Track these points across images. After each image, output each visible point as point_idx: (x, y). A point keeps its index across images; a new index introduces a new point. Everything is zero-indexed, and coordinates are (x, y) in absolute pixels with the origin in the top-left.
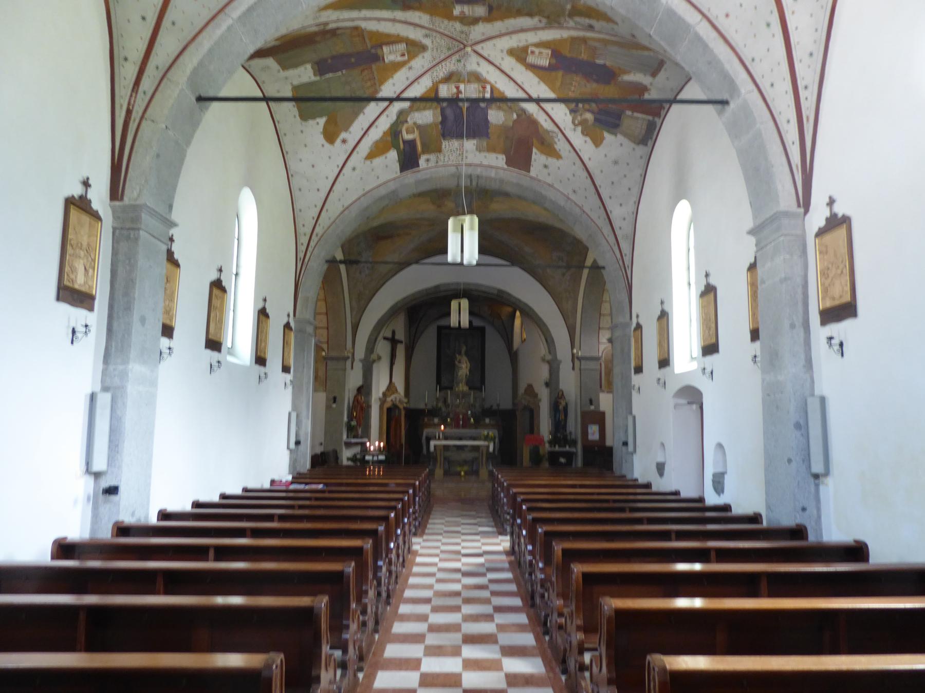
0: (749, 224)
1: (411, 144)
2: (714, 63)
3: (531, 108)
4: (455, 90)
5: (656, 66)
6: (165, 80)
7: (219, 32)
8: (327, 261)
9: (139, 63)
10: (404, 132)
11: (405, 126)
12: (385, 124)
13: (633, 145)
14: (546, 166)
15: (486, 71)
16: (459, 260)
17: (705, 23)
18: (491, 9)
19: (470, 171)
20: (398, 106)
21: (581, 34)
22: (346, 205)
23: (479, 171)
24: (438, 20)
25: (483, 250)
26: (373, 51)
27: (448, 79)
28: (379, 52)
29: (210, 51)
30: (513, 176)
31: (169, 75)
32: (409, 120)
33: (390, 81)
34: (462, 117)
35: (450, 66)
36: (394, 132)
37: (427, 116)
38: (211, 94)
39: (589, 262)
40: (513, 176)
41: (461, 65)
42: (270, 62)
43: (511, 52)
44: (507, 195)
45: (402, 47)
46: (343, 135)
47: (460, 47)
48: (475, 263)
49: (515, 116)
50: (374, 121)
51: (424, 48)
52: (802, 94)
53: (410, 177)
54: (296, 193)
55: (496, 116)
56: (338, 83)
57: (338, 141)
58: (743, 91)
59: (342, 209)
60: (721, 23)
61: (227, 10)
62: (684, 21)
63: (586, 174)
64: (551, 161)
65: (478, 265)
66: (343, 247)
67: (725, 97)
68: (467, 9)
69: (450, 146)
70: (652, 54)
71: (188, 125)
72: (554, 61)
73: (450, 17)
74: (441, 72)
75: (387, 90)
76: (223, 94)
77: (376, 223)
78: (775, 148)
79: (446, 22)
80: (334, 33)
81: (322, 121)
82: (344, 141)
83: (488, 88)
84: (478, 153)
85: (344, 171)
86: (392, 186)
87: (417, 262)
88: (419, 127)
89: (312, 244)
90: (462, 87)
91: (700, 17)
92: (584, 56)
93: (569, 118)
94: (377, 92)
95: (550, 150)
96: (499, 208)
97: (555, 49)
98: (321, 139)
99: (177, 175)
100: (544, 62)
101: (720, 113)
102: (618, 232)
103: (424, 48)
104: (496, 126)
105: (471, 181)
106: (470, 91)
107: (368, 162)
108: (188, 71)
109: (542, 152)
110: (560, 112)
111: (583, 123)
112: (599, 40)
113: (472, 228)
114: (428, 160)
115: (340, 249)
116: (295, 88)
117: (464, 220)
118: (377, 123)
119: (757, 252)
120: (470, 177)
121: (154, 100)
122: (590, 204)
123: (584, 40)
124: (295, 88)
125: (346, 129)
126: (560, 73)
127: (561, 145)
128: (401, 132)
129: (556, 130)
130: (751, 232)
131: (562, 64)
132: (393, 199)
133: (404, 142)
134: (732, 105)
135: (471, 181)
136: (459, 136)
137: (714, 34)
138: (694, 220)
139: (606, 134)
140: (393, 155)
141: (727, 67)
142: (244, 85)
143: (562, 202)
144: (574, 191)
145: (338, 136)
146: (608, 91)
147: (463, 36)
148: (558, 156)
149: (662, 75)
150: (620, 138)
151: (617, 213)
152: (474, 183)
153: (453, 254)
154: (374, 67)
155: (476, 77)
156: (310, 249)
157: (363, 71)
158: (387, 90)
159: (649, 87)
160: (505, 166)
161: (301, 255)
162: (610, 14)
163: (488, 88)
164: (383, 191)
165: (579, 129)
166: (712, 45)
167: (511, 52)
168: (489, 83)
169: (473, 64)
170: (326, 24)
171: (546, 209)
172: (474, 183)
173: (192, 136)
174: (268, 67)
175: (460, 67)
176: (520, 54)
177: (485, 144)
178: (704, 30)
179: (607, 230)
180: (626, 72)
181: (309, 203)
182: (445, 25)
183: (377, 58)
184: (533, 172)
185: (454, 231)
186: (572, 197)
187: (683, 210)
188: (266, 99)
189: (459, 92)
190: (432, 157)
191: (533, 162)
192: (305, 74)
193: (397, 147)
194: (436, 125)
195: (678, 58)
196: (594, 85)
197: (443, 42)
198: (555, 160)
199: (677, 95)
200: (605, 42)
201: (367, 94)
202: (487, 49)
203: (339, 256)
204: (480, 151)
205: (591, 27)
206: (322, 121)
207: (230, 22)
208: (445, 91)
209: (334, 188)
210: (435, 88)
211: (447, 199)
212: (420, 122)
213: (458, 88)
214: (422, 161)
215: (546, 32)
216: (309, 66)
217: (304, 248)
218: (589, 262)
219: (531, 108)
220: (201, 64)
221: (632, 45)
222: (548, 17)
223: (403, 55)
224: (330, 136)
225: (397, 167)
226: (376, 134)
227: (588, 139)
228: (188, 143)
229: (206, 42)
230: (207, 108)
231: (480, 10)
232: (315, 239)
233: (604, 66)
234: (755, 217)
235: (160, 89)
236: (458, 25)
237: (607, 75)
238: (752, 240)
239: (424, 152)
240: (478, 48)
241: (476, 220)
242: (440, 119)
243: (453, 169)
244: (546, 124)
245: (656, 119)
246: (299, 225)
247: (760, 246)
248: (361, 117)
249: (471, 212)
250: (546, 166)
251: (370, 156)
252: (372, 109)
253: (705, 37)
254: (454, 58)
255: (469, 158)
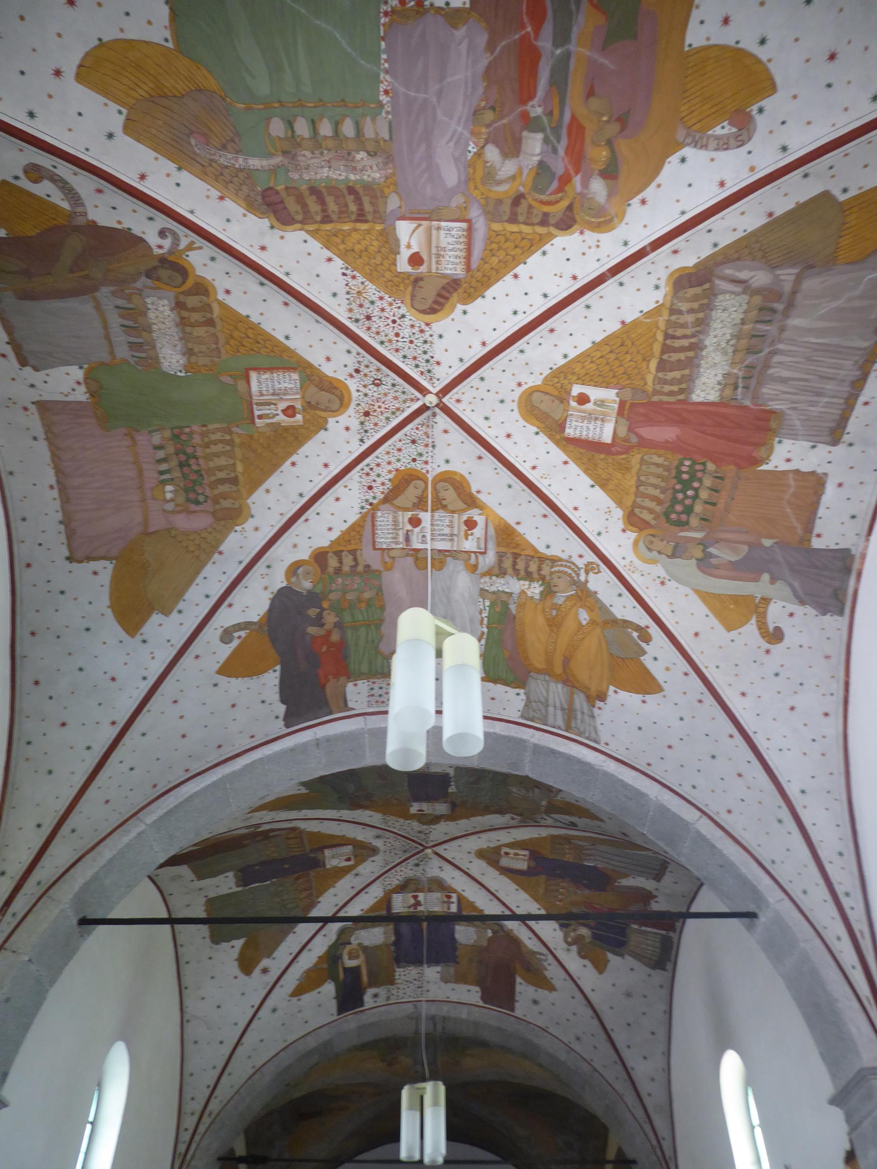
0: (828, 1089)
1: (354, 972)
2: (727, 865)
3: (512, 925)
4: (412, 901)
5: (660, 867)
6: (45, 898)
7: (126, 840)
8: (220, 1159)
9: (18, 878)
10: (345, 957)
11: (348, 948)
12: (321, 946)
13: (648, 970)
14: (535, 1002)
15: (449, 875)
16: (417, 1157)
17: (705, 820)
18: (454, 806)
19: (433, 1010)
20: (334, 928)
21: (563, 832)
22: (258, 1065)
23: (445, 1010)
24: (391, 819)
25: (453, 1134)
26: (312, 855)
27: (402, 888)
28: (319, 856)
29: (110, 861)
30: (491, 1017)
31: (51, 892)
32: (352, 940)
33: (332, 891)
34: (423, 937)
35: (406, 872)
36: (332, 956)
37: (375, 936)
38: (99, 915)
39: (611, 1154)
40: (491, 1017)
41: (420, 869)
42: (184, 870)
43: (481, 854)
44: (483, 1044)
45: (348, 849)
46: (265, 963)
47: (418, 849)
48: (440, 1160)
49: (490, 933)
50: (304, 947)
51: (374, 851)
52: (846, 902)
53: (352, 1021)
54: (189, 1047)
55: (464, 934)
56: (266, 897)
57: (257, 971)
58: (771, 900)
59: (252, 1071)
60: (724, 819)
61: (139, 815)
62: (682, 820)
63: (590, 1012)
64: (542, 994)
65: (447, 1161)
66: (247, 1131)
67: (751, 908)
68: (426, 807)
69: (405, 974)
70: (650, 854)
71: (58, 955)
72: (533, 864)
73: (407, 816)
74: (395, 878)
75: (325, 906)
76: (111, 916)
77: (297, 1094)
78: (832, 975)
79: (401, 820)
80: (266, 835)
81: (239, 943)
82: (265, 971)
83: (454, 898)
84: (443, 984)
85: (261, 1014)
86: (325, 1035)
87: (350, 1160)
88: (365, 949)
89: (202, 1129)
90: (421, 896)
91: (699, 814)
92: (569, 858)
93: (559, 934)
94: (313, 905)
95: (540, 981)
96: (473, 1065)
97: (532, 848)
98: (234, 968)
99: (25, 1028)
100: (523, 865)
101: (750, 928)
102: (647, 1101)
103: (374, 851)
104: (466, 945)
105: (435, 1024)
106: (432, 903)
107: (295, 999)
108: (76, 888)
109: (530, 982)
110: (550, 930)
111: (577, 941)
112: (584, 839)
113: (435, 1104)
114: (376, 996)
115: (242, 1137)
116: (211, 903)
117: (424, 1089)
118: (309, 946)
119: (850, 1133)
120: (433, 1019)
121: (24, 924)
122: (602, 1058)
123: (567, 839)
124: (211, 903)
125: (269, 955)
126: (542, 878)
127: (552, 972)
128: (340, 957)
129: (545, 951)
130: (835, 1101)
131: (543, 868)
132: (326, 1055)
133: (346, 970)
134: (762, 919)
135: (435, 1024)
136: (417, 961)
137: (720, 833)
138: (751, 1080)
139: (610, 956)
140: (329, 989)
141: (744, 870)
142: (144, 900)
143: (563, 1056)
144: (578, 1039)
145: (258, 962)
146: (604, 900)
147: (422, 836)
148: (552, 988)
149: (668, 879)
150: (629, 961)
151: (642, 1069)
152: (439, 1027)
153: (407, 1148)
154: (312, 873)
155: (439, 885)
156: (197, 1138)
157: (297, 879)
158: (325, 906)
159: (655, 893)
160: (481, 1004)
161: (182, 1148)
162: (593, 811)
163: (454, 898)
164: (312, 1043)
165: (574, 948)
166: (719, 845)
167: (481, 854)
168: (455, 891)
169: (434, 869)
170: (258, 825)
171: (541, 1066)
172: (439, 1027)
173: (60, 971)
174: (180, 877)
175: (417, 873)
176: (491, 856)
177: (452, 970)
178: (705, 827)
179: (630, 1098)
180: (626, 876)
181: (207, 1059)
182: (399, 824)
183: (317, 863)
184: (519, 1012)
185: (411, 1108)
186: (576, 1046)
187: (731, 1066)
188: (171, 921)
189: (418, 904)
190: (382, 991)
191: (518, 997)
192: (225, 884)
193: (334, 978)
194: (387, 945)
195: (683, 861)
196: (587, 892)
197: (399, 843)
198: (546, 992)
199: (689, 906)
200: (594, 841)
201: (300, 914)
202: (450, 851)
203: (240, 1150)
204: (446, 982)
205: (573, 825)
206: (239, 943)
207: (142, 827)
208: (400, 904)
209: (244, 1040)
210: (386, 901)
211: (401, 1055)
212: (366, 943)
213: (415, 897)
214: (368, 998)
215: (522, 830)
216: (231, 874)
217: (198, 1106)
218: (611, 1154)
219: (512, 925)
220: (95, 878)
221: (624, 843)
222: (520, 815)
223: (348, 860)
224: (247, 964)
225: (333, 1005)
226: (308, 960)
227: (586, 962)
228: (53, 981)
229: (107, 852)
230: (89, 933)
231: (441, 808)
232: (206, 1120)
233: (595, 868)
234: (834, 1075)
235: (35, 909)
236: (415, 824)
237: (600, 880)
238: (837, 1115)
239: (373, 983)
240: (440, 849)
241: (442, 1088)
242: (393, 938)
243: (409, 1008)
244: (531, 943)
245: (671, 934)
246: (187, 1097)
247: (853, 1127)
248: (291, 938)
249: (434, 1077)
250: (535, 1002)
251: (298, 992)
252: (304, 930)
253: (709, 837)
254: (412, 861)
255: (432, 991)
